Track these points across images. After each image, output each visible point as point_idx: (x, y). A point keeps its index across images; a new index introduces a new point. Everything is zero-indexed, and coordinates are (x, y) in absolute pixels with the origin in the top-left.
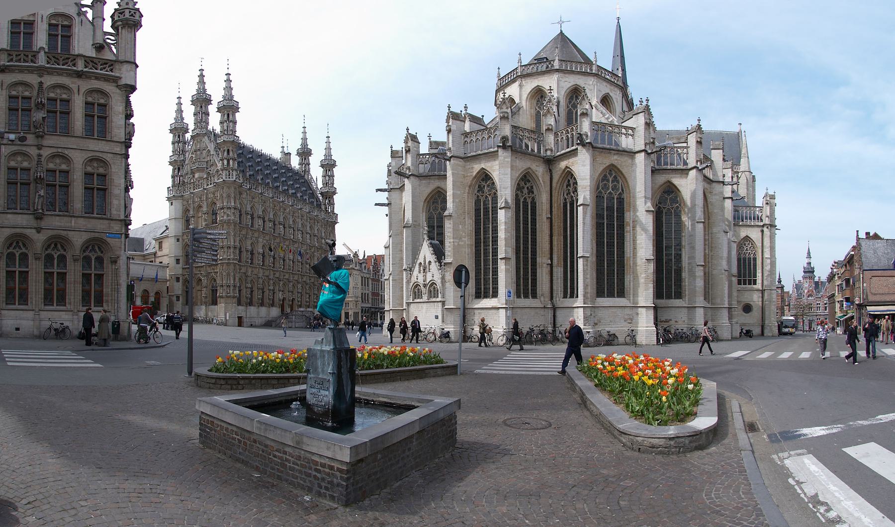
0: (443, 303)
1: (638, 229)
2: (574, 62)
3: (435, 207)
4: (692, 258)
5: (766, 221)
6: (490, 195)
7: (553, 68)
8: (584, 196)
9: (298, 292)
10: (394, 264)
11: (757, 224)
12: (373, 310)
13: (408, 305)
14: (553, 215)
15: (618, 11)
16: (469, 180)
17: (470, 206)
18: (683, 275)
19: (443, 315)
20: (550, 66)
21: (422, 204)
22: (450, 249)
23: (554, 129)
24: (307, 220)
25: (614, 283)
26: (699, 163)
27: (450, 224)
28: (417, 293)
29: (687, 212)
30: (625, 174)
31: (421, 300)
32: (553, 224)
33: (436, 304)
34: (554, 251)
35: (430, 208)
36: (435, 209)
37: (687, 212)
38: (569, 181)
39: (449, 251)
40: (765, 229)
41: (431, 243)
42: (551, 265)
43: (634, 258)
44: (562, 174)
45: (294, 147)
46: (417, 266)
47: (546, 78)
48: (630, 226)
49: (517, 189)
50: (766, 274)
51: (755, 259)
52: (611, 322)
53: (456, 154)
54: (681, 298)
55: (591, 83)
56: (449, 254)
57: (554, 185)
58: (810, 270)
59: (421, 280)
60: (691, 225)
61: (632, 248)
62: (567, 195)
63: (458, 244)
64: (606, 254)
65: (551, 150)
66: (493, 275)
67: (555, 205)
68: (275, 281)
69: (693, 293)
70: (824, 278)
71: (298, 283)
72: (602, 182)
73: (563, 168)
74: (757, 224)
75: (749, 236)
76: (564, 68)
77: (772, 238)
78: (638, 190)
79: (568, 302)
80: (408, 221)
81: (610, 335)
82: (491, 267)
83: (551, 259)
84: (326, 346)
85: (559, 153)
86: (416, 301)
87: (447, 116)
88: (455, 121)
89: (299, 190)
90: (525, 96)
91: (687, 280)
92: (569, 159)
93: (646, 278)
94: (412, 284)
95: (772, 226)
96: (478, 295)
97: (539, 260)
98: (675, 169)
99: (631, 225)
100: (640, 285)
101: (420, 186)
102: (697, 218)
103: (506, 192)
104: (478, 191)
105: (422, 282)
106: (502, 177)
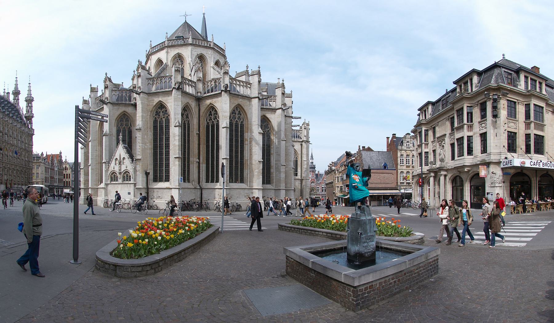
0: (135, 185)
1: (253, 143)
2: (198, 39)
3: (122, 124)
4: (278, 160)
5: (305, 139)
6: (164, 118)
7: (188, 43)
8: (226, 122)
9: (14, 176)
10: (92, 159)
11: (298, 140)
12: (51, 187)
14: (200, 132)
15: (204, 9)
16: (151, 108)
17: (151, 124)
18: (272, 170)
19: (135, 192)
20: (186, 41)
21: (114, 121)
22: (140, 150)
23: (202, 80)
24: (6, 126)
25: (238, 174)
26: (283, 106)
27: (140, 134)
28: (113, 178)
29: (274, 134)
30: (245, 110)
31: (117, 182)
33: (128, 185)
34: (201, 154)
35: (118, 124)
36: (122, 125)
37: (274, 134)
38: (211, 112)
39: (139, 152)
40: (303, 143)
41: (124, 146)
42: (199, 163)
43: (250, 160)
44: (207, 107)
45: (11, 89)
46: (114, 160)
47: (184, 48)
48: (248, 141)
50: (304, 170)
52: (237, 197)
53: (143, 91)
54: (270, 184)
55: (210, 53)
56: (139, 153)
57: (201, 114)
58: (313, 167)
59: (117, 169)
60: (278, 142)
61: (249, 154)
62: (209, 120)
63: (145, 148)
64: (234, 157)
65: (201, 93)
66: (165, 168)
67: (201, 126)
68: (3, 168)
69: (279, 181)
70: (322, 172)
71: (14, 170)
72: (232, 114)
73: (208, 104)
74: (298, 140)
76: (194, 43)
77: (308, 148)
78: (253, 120)
79: (210, 185)
80: (106, 131)
81: (238, 205)
82: (164, 162)
83: (199, 159)
84: (368, 216)
85: (205, 95)
86: (112, 182)
87: (137, 67)
88: (143, 70)
89: (10, 107)
90: (170, 59)
91: (274, 173)
92: (212, 99)
93: (259, 172)
94: (109, 172)
95: (308, 142)
96: (155, 180)
97: (191, 159)
98: (268, 109)
99: (249, 140)
100: (255, 176)
101: (113, 110)
102: (282, 138)
103: (179, 117)
104: (156, 115)
105: (118, 171)
106: (175, 107)
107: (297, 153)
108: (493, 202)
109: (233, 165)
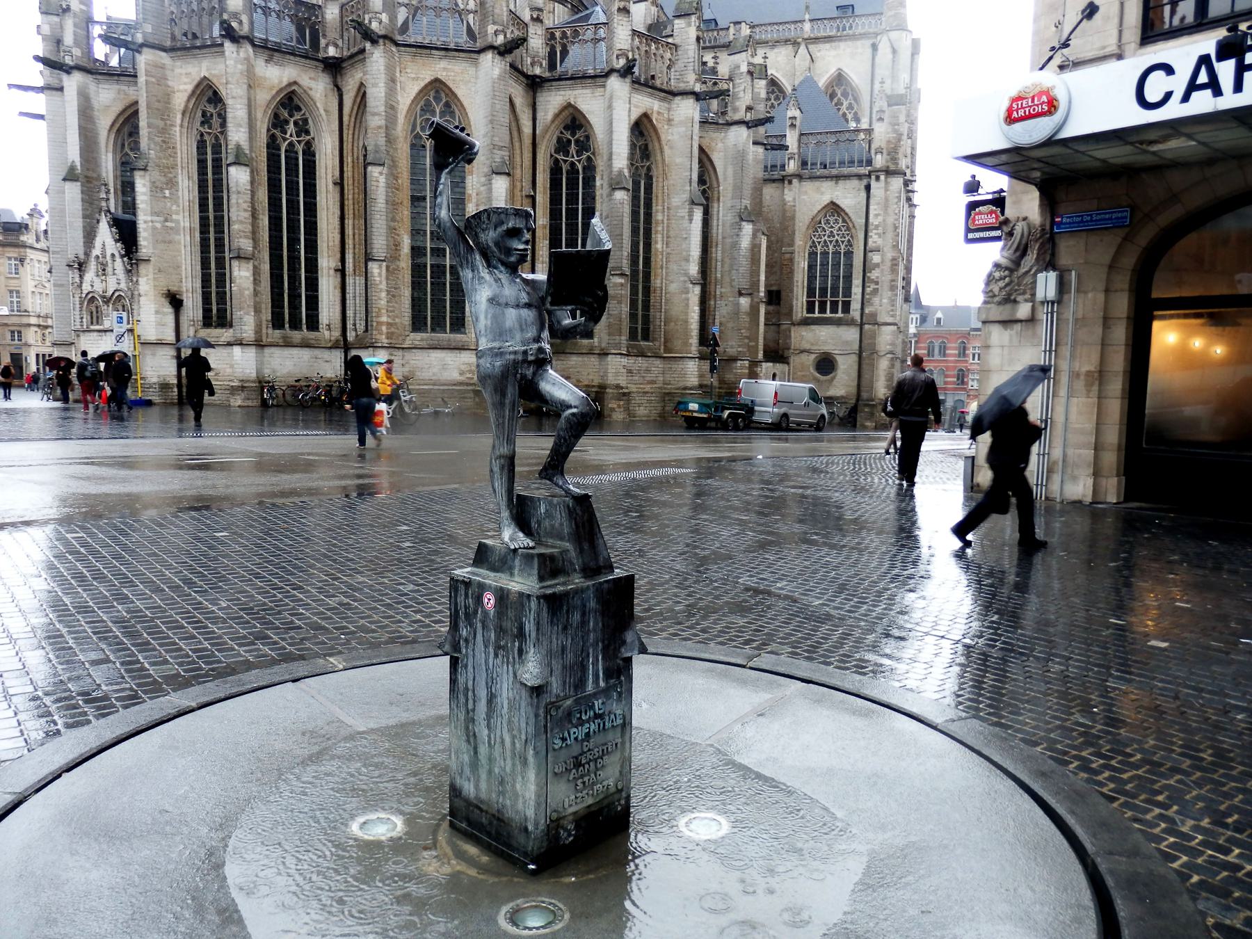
13: (78, 336)
32: (346, 197)
49: (275, 126)
51: (849, 254)
57: (346, 118)
75: (837, 202)
83: (343, 260)
86: (92, 327)
104: (203, 123)
107: (851, 225)
108: (115, 333)
109: (426, 277)
